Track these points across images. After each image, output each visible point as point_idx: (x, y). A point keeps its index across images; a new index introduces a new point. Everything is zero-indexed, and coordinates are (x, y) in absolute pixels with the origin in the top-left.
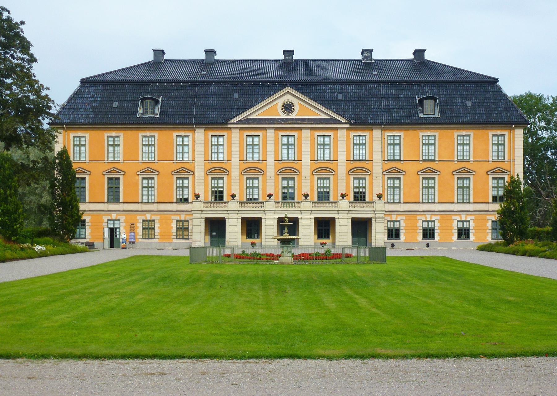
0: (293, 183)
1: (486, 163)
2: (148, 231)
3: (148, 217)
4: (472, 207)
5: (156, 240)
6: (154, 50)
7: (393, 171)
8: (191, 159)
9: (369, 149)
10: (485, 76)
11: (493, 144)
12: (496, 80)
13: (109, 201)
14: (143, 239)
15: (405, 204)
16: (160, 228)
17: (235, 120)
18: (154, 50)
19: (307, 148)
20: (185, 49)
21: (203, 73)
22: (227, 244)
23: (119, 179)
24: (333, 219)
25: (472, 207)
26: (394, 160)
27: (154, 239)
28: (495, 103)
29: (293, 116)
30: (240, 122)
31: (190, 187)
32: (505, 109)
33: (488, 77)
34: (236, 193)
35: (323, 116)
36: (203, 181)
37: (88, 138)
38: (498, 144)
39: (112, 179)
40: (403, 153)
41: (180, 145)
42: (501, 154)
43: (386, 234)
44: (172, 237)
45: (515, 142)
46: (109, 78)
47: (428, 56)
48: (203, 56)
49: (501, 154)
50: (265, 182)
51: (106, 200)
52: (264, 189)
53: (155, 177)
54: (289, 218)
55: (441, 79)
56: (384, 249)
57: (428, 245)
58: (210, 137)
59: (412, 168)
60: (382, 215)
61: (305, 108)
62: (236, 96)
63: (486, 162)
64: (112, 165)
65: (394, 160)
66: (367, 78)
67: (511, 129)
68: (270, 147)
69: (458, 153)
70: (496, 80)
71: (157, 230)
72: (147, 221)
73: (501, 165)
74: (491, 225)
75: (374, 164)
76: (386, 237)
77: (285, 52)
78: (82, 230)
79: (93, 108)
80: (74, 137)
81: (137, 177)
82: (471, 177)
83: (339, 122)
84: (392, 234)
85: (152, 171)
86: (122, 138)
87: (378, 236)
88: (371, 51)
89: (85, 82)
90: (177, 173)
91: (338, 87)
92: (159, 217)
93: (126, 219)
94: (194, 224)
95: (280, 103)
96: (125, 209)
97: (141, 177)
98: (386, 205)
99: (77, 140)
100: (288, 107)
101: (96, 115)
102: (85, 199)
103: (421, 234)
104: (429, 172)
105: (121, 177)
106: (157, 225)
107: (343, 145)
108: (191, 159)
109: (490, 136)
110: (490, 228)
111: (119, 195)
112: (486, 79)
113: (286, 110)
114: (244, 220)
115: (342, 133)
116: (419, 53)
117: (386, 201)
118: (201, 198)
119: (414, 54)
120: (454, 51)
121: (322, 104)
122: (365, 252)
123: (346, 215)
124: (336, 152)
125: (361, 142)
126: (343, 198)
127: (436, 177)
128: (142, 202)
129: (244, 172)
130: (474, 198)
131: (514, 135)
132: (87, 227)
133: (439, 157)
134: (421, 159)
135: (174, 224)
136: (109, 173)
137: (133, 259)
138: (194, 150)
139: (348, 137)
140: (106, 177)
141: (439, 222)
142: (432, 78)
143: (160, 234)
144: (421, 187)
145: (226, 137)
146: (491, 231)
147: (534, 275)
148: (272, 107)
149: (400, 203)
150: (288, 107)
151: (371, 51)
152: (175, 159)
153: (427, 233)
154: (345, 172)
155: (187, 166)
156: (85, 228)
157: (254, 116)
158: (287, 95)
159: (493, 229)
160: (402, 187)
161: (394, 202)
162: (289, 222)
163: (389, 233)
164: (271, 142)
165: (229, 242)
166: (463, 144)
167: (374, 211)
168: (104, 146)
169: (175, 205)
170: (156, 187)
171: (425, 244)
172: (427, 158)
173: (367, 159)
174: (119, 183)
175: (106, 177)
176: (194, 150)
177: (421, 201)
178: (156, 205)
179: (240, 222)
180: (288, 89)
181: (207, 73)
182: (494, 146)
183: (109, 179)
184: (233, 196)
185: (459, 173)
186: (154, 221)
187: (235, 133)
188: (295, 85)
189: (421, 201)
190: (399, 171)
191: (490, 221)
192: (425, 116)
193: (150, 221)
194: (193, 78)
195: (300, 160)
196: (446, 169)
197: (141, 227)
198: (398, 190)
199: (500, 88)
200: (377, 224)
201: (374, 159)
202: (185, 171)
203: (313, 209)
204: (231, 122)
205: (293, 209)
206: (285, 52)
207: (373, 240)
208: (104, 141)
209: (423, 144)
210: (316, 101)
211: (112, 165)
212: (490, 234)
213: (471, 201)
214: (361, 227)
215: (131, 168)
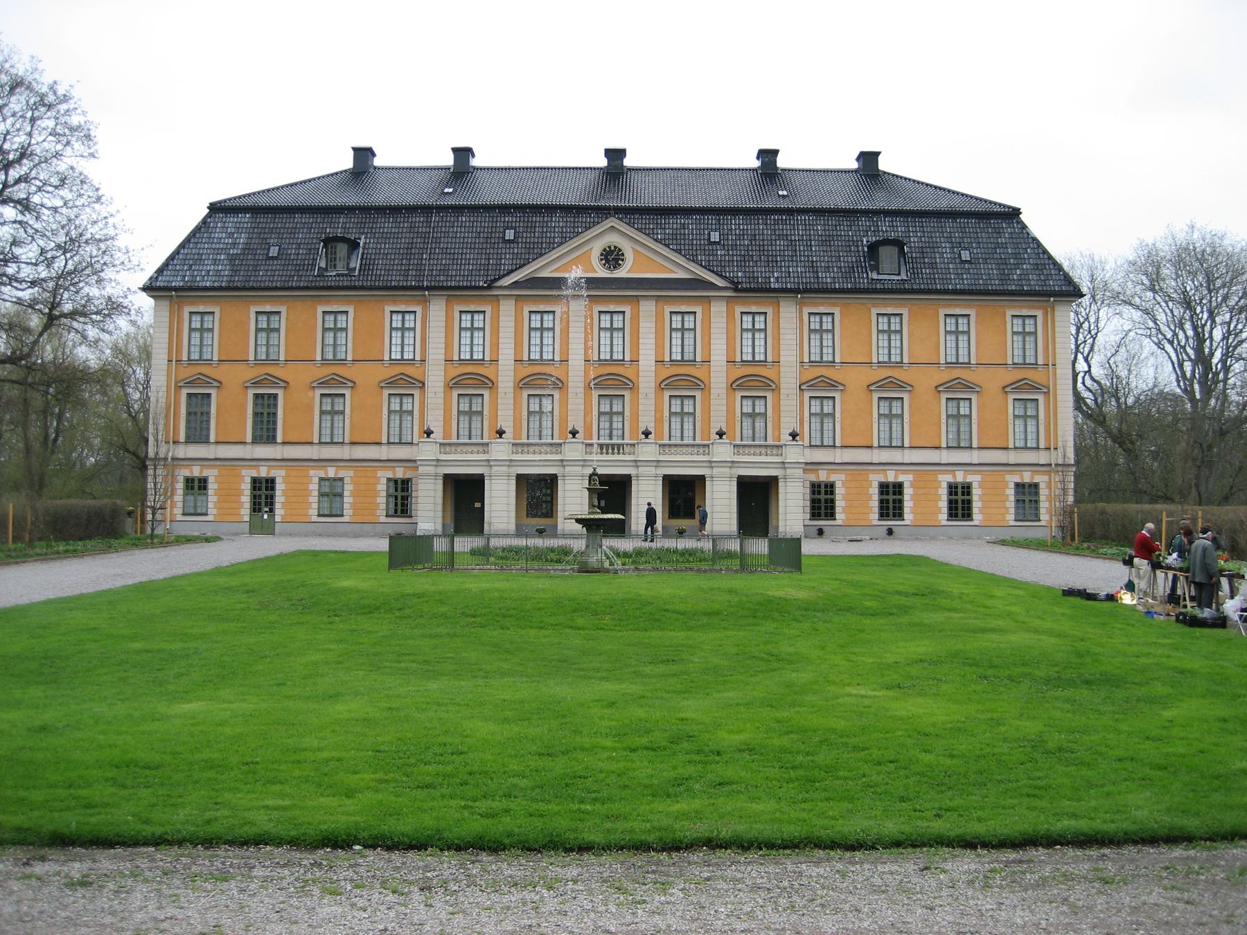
0: (620, 406)
1: (1001, 371)
2: (331, 503)
3: (331, 472)
4: (975, 457)
5: (210, 518)
6: (355, 149)
7: (820, 384)
8: (418, 358)
9: (773, 339)
10: (995, 203)
11: (1014, 333)
12: (1016, 212)
13: (256, 440)
14: (184, 514)
15: (845, 450)
16: (353, 495)
17: (507, 281)
18: (355, 149)
19: (649, 337)
20: (413, 145)
21: (446, 190)
22: (486, 527)
23: (275, 396)
24: (702, 479)
25: (975, 457)
26: (612, 359)
27: (206, 514)
28: (1016, 256)
29: (622, 273)
30: (516, 285)
31: (416, 412)
32: (1036, 266)
33: (1000, 205)
34: (507, 425)
35: (681, 275)
36: (442, 401)
37: (419, 315)
38: (1024, 334)
39: (262, 395)
40: (838, 347)
41: (950, 332)
42: (759, 349)
43: (808, 510)
44: (379, 513)
45: (1057, 329)
46: (263, 201)
47: (884, 165)
48: (603, 162)
49: (1030, 353)
50: (564, 403)
51: (249, 439)
52: (564, 420)
53: (347, 393)
54: (600, 476)
55: (910, 207)
56: (796, 542)
57: (890, 532)
58: (457, 315)
59: (925, 380)
60: (799, 472)
61: (644, 258)
62: (510, 235)
63: (863, 368)
64: (399, 369)
65: (542, 360)
66: (768, 204)
67: (425, 302)
68: (576, 335)
69: (947, 349)
70: (1016, 212)
71: (348, 500)
72: (328, 479)
73: (1030, 374)
74: (1012, 492)
75: (782, 369)
76: (808, 516)
77: (609, 153)
78: (200, 498)
79: (232, 259)
80: (392, 312)
81: (310, 394)
82: (974, 397)
83: (712, 286)
84: (956, 509)
85: (340, 381)
86: (284, 315)
87: (791, 513)
88: (776, 152)
89: (215, 208)
90: (324, 384)
91: (712, 219)
92: (351, 473)
93: (288, 476)
94: (420, 487)
95: (597, 248)
96: (286, 456)
97: (318, 392)
98: (807, 451)
99: (197, 318)
100: (612, 257)
101: (235, 271)
102: (208, 436)
103: (877, 510)
104: (890, 387)
105: (280, 392)
106: (348, 488)
107: (720, 334)
108: (418, 358)
109: (1009, 319)
110: (1012, 498)
111: (275, 430)
112: (997, 209)
113: (607, 261)
114: (520, 478)
115: (718, 310)
116: (869, 159)
117: (807, 443)
118: (438, 436)
119: (858, 159)
120: (937, 156)
121: (679, 251)
122: (760, 546)
123: (505, 469)
124: (496, 345)
125: (893, 328)
126: (721, 437)
127: (906, 396)
128: (320, 443)
129: (735, 385)
130: (979, 439)
131: (1053, 315)
132: (210, 492)
133: (910, 356)
134: (1010, 362)
135: (314, 487)
136: (257, 384)
137: (853, 561)
138: (424, 340)
139: (730, 315)
140: (185, 392)
141: (285, 481)
142: (894, 205)
143: (354, 506)
144: (875, 415)
145: (488, 315)
146: (316, 499)
147: (84, 591)
148: (578, 261)
149: (971, 447)
150: (612, 257)
151: (776, 152)
152: (875, 360)
153: (888, 508)
154: (653, 385)
155: (410, 370)
156: (206, 494)
157: (546, 274)
158: (611, 234)
159: (1017, 501)
160: (838, 415)
161: (822, 446)
162: (601, 484)
163: (813, 508)
164: (578, 324)
165: (490, 524)
166: (957, 333)
167: (783, 463)
168: (248, 331)
169: (249, 447)
170: (348, 411)
171: (814, 531)
172: (886, 359)
173: (770, 359)
174: (275, 406)
175: (251, 392)
176: (424, 340)
177: (1011, 446)
178: (347, 448)
179: (440, 482)
180: (612, 222)
181: (455, 190)
182: (1015, 338)
183: (256, 396)
184: (501, 433)
185: (949, 389)
186: (341, 479)
187: (507, 309)
188: (629, 213)
189: (1011, 446)
190: (900, 385)
191: (1012, 485)
192: (881, 277)
193: (335, 480)
194: (431, 201)
195: (635, 361)
196: (925, 380)
197: (316, 493)
198: (831, 420)
199: (1024, 227)
200: (567, 487)
201: (782, 359)
202: (405, 382)
203: (736, 458)
204: (499, 284)
205: (621, 457)
206: (609, 153)
207: (781, 523)
208: (248, 324)
209: (879, 331)
210: (667, 246)
211: (399, 369)
212: (1012, 511)
213: (906, 444)
214: (756, 497)
215: (299, 376)
